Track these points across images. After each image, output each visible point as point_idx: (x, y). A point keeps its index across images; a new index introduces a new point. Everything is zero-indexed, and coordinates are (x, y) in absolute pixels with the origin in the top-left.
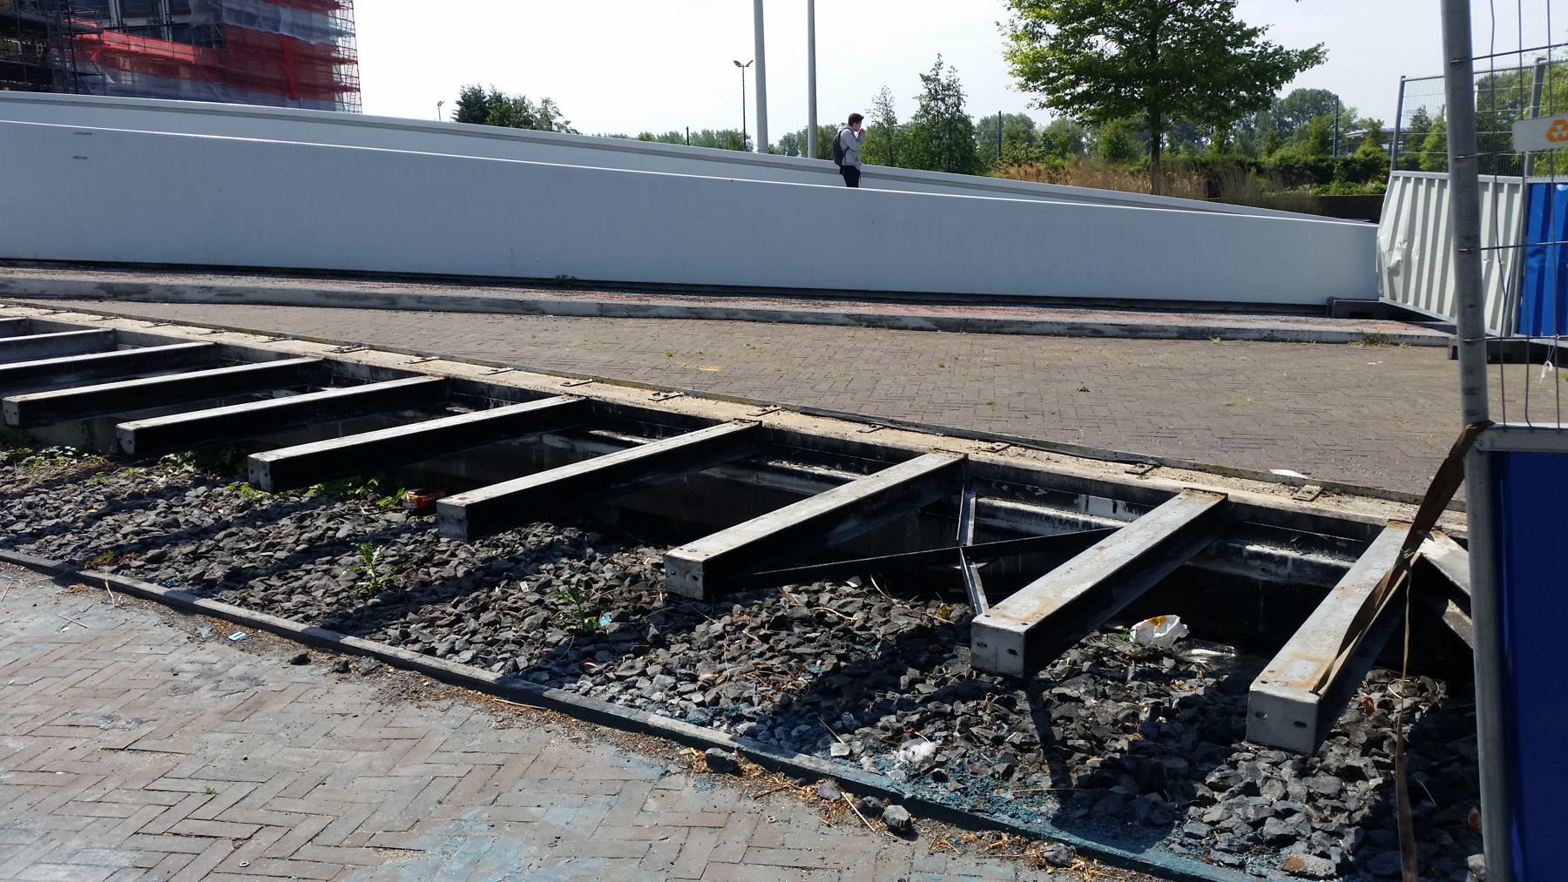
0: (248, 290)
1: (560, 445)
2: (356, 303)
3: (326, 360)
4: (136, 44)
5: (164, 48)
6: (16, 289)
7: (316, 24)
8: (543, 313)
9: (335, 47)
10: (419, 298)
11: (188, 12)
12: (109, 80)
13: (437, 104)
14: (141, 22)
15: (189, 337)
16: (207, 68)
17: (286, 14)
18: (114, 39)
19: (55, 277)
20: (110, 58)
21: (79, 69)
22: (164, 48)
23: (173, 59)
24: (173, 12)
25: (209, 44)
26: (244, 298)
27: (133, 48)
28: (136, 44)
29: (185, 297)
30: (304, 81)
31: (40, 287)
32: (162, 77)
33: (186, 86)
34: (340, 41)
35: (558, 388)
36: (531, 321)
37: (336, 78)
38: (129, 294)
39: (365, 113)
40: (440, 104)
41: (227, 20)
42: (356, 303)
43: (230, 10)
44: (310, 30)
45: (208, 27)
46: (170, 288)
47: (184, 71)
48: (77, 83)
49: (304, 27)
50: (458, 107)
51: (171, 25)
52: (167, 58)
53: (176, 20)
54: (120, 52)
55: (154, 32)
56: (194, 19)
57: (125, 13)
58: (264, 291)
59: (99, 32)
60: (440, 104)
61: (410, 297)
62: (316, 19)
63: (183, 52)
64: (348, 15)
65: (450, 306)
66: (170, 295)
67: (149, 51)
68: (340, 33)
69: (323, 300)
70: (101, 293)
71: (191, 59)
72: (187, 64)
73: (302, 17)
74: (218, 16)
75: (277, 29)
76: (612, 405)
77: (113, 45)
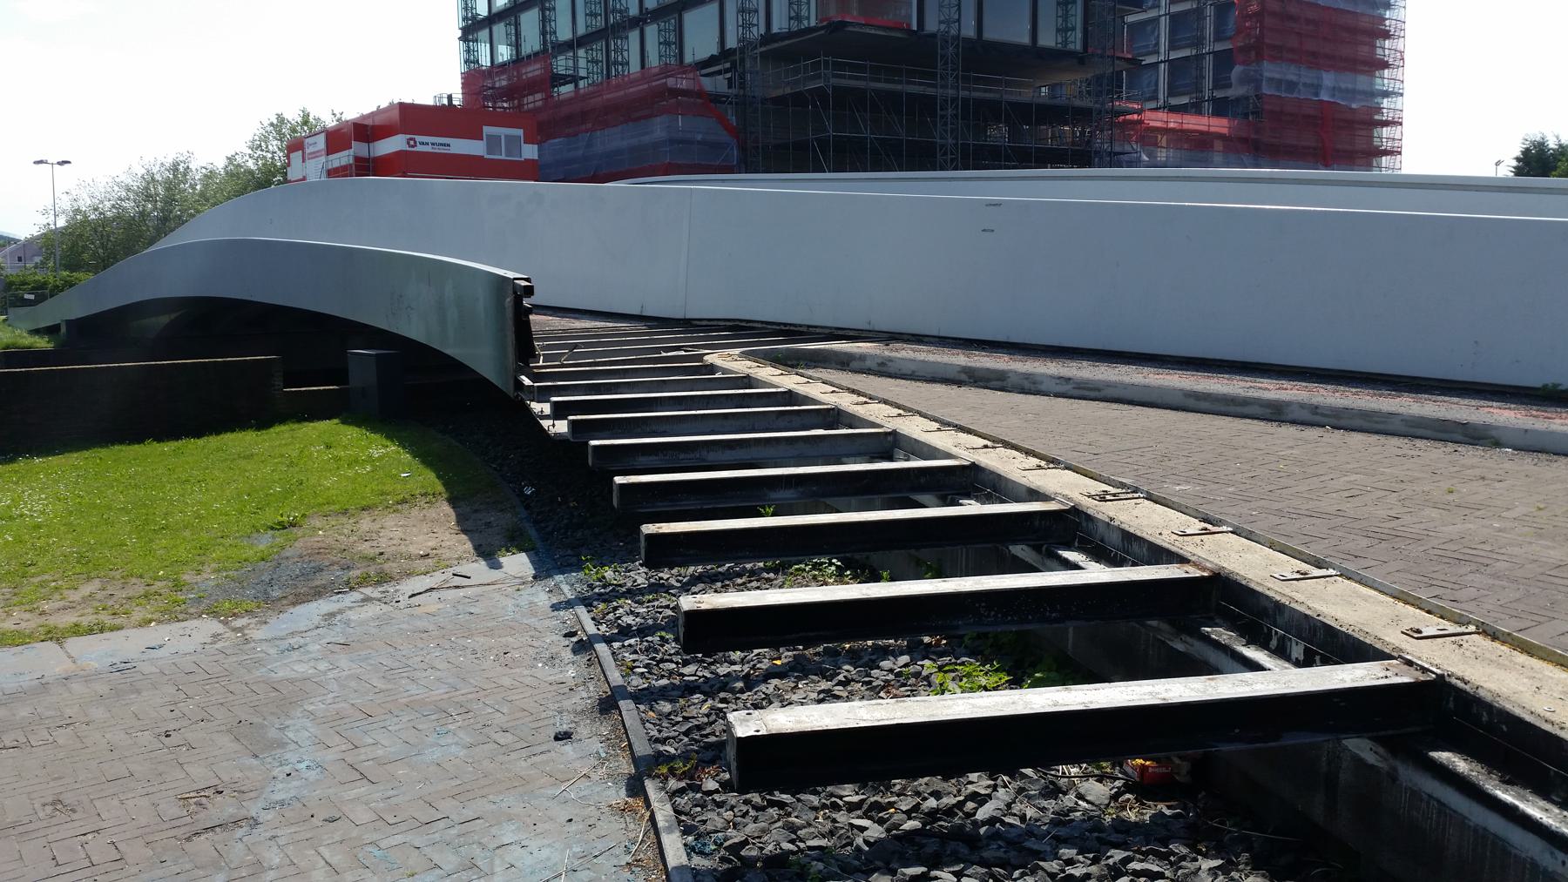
0: (1109, 385)
1: (1371, 758)
2: (1232, 409)
3: (1076, 511)
4: (1174, 121)
5: (1193, 122)
6: (892, 368)
7: (1360, 87)
8: (1497, 444)
9: (1379, 110)
10: (1315, 409)
11: (1229, 86)
12: (1145, 158)
13: (1490, 155)
14: (1185, 100)
15: (954, 451)
16: (1245, 140)
17: (1328, 79)
18: (1156, 119)
19: (931, 358)
20: (1149, 137)
21: (1117, 149)
22: (1193, 122)
23: (1208, 133)
24: (1216, 86)
25: (1246, 115)
26: (1102, 394)
27: (1172, 125)
28: (1174, 121)
29: (1043, 388)
30: (1339, 146)
31: (913, 367)
32: (1197, 148)
33: (1218, 158)
34: (1385, 103)
35: (1393, 638)
36: (1471, 456)
37: (1376, 142)
38: (989, 380)
39: (1403, 172)
40: (1497, 164)
41: (1266, 90)
42: (1232, 409)
43: (1271, 80)
44: (1353, 93)
45: (1247, 98)
46: (1028, 376)
47: (1218, 145)
48: (1114, 159)
49: (1347, 91)
50: (1515, 163)
51: (1213, 100)
52: (1201, 133)
53: (1218, 94)
54: (1157, 129)
55: (1195, 108)
56: (1235, 92)
57: (1172, 92)
58: (1126, 386)
59: (1139, 112)
60: (1497, 164)
61: (1302, 406)
62: (1361, 81)
63: (1219, 125)
64: (1398, 73)
65: (1358, 422)
66: (1027, 385)
67: (1185, 126)
68: (1386, 94)
69: (1191, 402)
70: (963, 377)
71: (1225, 131)
72: (1221, 136)
73: (1346, 81)
74: (1258, 87)
75: (1317, 94)
76: (1489, 707)
77: (1152, 124)
